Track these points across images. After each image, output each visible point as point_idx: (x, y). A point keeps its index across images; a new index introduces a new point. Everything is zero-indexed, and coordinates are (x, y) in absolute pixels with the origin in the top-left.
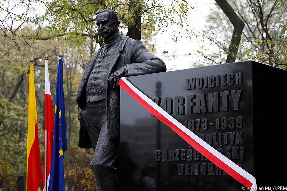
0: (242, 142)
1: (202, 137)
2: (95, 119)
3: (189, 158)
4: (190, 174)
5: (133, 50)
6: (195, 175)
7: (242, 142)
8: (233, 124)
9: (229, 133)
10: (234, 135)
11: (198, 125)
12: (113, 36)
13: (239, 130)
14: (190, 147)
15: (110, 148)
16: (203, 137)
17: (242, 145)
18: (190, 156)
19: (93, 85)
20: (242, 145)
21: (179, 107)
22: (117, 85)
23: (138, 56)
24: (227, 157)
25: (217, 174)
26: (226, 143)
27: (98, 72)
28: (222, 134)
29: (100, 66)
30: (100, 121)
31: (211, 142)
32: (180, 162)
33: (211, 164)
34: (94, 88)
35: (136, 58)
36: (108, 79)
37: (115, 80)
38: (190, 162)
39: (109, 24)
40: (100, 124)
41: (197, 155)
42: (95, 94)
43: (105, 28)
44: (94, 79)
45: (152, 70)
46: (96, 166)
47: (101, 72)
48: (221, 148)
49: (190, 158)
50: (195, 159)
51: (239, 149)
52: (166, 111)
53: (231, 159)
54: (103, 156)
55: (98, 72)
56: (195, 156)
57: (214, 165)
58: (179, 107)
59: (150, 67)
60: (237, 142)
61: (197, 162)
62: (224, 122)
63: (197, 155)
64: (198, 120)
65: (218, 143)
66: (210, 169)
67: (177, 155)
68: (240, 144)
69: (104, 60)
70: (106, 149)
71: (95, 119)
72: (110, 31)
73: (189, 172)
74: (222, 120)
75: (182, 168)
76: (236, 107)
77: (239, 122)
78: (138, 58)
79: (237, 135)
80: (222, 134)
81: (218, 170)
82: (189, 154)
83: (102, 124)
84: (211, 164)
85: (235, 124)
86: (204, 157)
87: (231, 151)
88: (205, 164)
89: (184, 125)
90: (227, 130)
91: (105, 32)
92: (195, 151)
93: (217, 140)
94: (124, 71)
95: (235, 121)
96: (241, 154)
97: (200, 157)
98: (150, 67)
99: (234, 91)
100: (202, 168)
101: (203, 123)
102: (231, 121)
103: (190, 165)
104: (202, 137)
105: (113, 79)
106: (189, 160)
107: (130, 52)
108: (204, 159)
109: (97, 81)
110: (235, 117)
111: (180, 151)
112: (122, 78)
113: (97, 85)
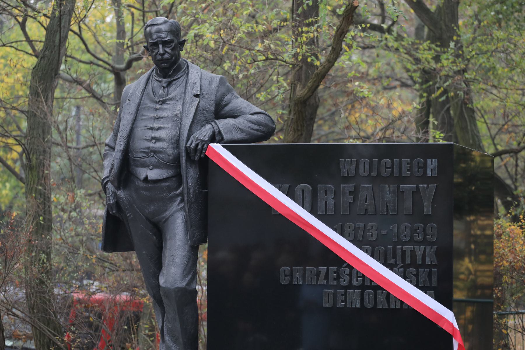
0: (435, 262)
1: (367, 250)
2: (152, 208)
3: (344, 281)
4: (346, 305)
5: (219, 94)
6: (354, 306)
7: (435, 262)
8: (420, 235)
9: (414, 248)
10: (423, 250)
11: (360, 232)
12: (176, 64)
13: (431, 244)
14: (345, 265)
15: (192, 259)
16: (369, 251)
17: (435, 266)
18: (346, 279)
19: (151, 151)
20: (435, 266)
21: (326, 202)
22: (202, 156)
23: (226, 105)
24: (411, 282)
25: (392, 307)
26: (408, 262)
27: (159, 129)
28: (402, 249)
29: (159, 118)
30: (165, 211)
31: (383, 258)
32: (327, 286)
33: (382, 292)
34: (153, 156)
35: (223, 108)
36: (186, 143)
37: (200, 147)
38: (346, 288)
39: (173, 46)
40: (164, 218)
41: (358, 277)
42: (155, 166)
43: (166, 52)
44: (154, 141)
45: (259, 133)
46: (176, 290)
47: (164, 128)
48: (401, 269)
49: (346, 281)
50: (355, 283)
51: (430, 271)
52: (303, 207)
53: (417, 286)
54: (185, 273)
55: (159, 129)
56: (355, 279)
57: (388, 294)
58: (326, 202)
59: (256, 127)
60: (428, 261)
61: (357, 288)
62: (405, 231)
63: (358, 277)
64: (362, 225)
65: (396, 262)
66: (381, 298)
67: (322, 275)
68: (431, 266)
69: (165, 106)
70: (188, 262)
71: (152, 208)
72: (174, 58)
73: (342, 302)
74: (402, 228)
75: (331, 297)
76: (427, 210)
77: (432, 231)
78: (227, 109)
79: (427, 251)
80: (402, 249)
81: (395, 302)
82: (343, 276)
83: (168, 218)
84: (382, 292)
85: (425, 235)
86: (371, 281)
87: (417, 275)
88: (332, 291)
89: (335, 230)
90: (412, 241)
91: (167, 59)
92: (356, 271)
93: (394, 257)
94: (214, 133)
95: (424, 230)
96: (435, 279)
97: (364, 281)
98: (256, 127)
99: (425, 185)
100: (366, 298)
101: (370, 229)
102: (418, 229)
103: (346, 293)
104: (367, 250)
105: (197, 145)
106: (344, 284)
107: (213, 97)
108: (370, 285)
109: (159, 145)
110: (425, 225)
111: (328, 270)
112: (212, 145)
113: (160, 152)
